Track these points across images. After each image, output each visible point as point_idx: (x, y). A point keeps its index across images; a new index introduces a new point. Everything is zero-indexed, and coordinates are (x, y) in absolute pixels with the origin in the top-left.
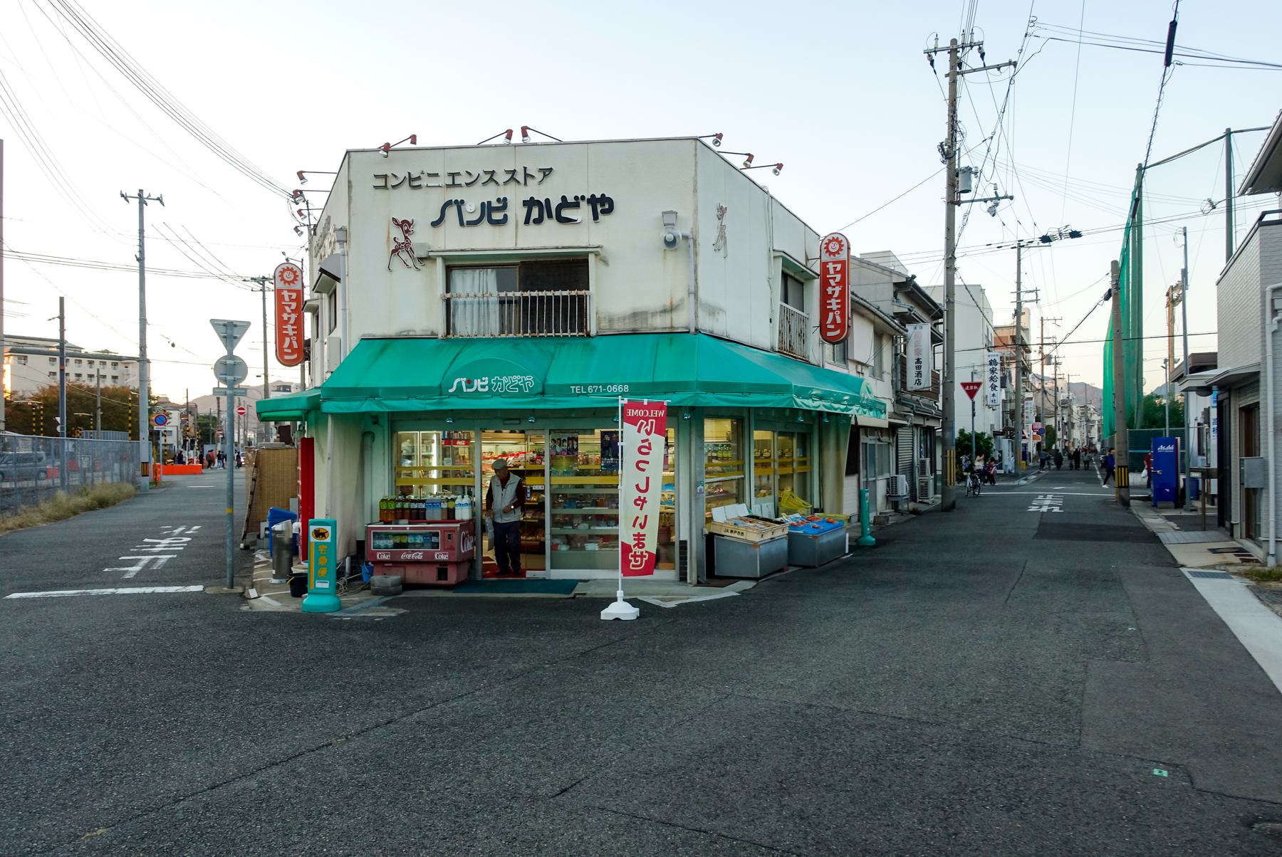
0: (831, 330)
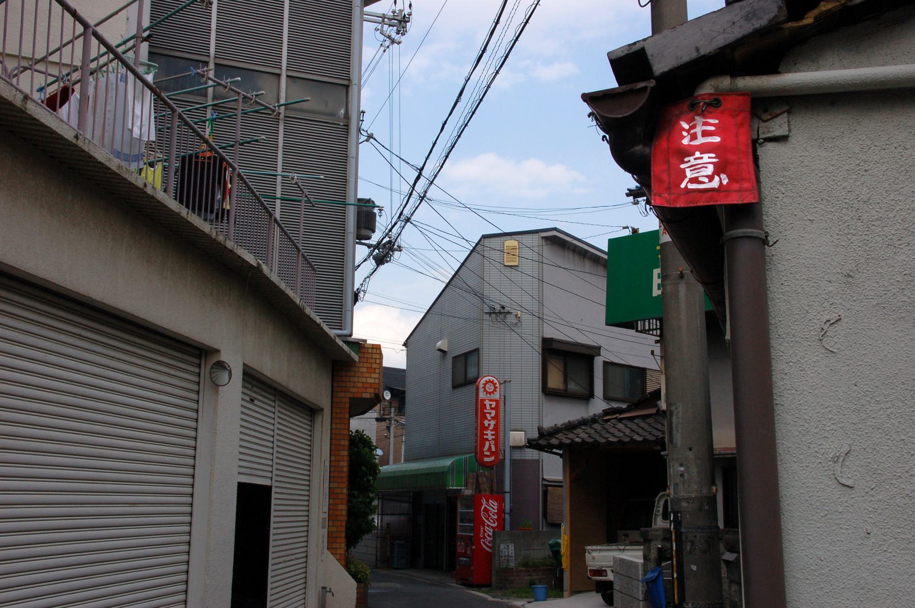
0: (487, 456)
